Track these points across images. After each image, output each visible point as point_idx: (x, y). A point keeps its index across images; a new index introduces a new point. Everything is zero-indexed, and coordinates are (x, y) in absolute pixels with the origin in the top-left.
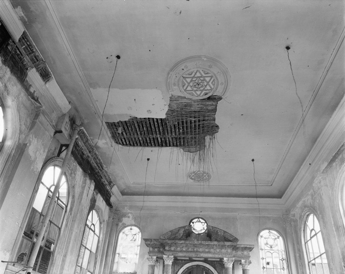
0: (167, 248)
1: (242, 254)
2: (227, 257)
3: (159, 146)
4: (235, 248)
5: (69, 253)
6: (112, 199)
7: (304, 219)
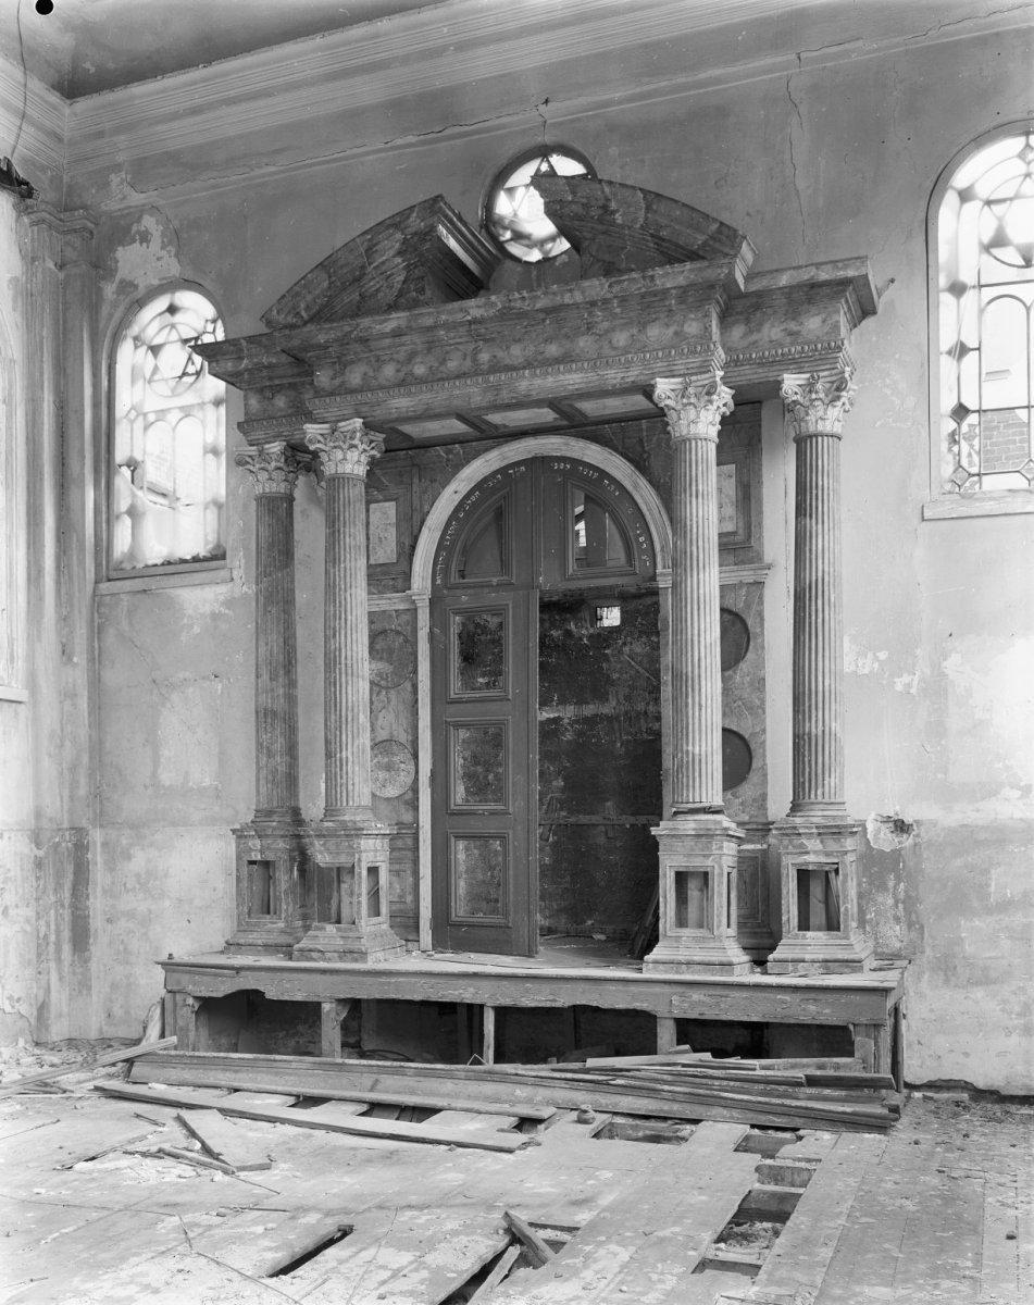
0: (323, 378)
1: (788, 339)
2: (680, 368)
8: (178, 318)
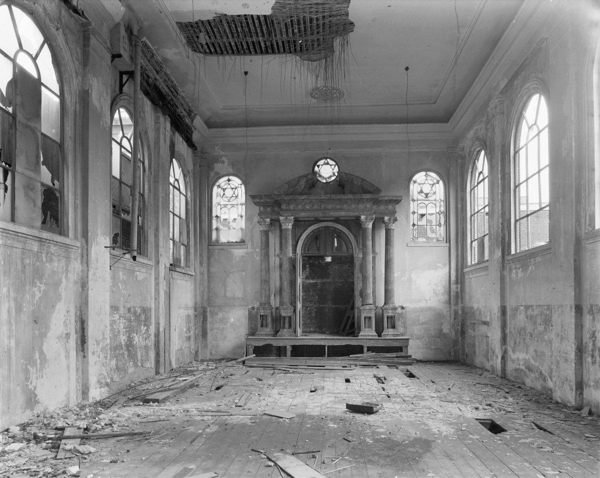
0: (284, 207)
3: (262, 53)
4: (377, 202)
5: (160, 226)
6: (195, 137)
7: (473, 156)
8: (230, 182)
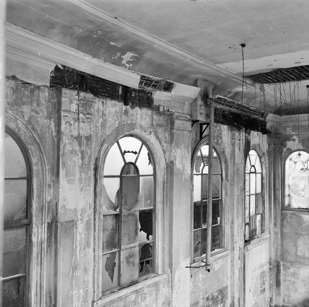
5: (235, 219)
